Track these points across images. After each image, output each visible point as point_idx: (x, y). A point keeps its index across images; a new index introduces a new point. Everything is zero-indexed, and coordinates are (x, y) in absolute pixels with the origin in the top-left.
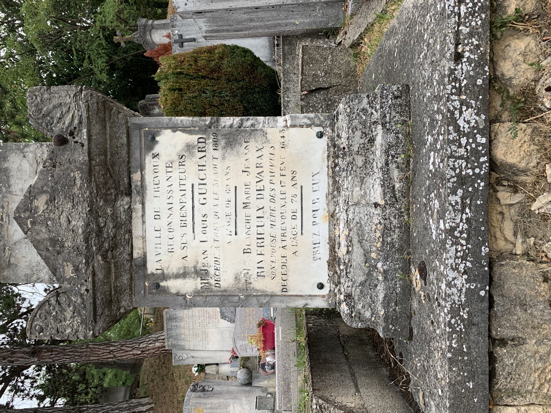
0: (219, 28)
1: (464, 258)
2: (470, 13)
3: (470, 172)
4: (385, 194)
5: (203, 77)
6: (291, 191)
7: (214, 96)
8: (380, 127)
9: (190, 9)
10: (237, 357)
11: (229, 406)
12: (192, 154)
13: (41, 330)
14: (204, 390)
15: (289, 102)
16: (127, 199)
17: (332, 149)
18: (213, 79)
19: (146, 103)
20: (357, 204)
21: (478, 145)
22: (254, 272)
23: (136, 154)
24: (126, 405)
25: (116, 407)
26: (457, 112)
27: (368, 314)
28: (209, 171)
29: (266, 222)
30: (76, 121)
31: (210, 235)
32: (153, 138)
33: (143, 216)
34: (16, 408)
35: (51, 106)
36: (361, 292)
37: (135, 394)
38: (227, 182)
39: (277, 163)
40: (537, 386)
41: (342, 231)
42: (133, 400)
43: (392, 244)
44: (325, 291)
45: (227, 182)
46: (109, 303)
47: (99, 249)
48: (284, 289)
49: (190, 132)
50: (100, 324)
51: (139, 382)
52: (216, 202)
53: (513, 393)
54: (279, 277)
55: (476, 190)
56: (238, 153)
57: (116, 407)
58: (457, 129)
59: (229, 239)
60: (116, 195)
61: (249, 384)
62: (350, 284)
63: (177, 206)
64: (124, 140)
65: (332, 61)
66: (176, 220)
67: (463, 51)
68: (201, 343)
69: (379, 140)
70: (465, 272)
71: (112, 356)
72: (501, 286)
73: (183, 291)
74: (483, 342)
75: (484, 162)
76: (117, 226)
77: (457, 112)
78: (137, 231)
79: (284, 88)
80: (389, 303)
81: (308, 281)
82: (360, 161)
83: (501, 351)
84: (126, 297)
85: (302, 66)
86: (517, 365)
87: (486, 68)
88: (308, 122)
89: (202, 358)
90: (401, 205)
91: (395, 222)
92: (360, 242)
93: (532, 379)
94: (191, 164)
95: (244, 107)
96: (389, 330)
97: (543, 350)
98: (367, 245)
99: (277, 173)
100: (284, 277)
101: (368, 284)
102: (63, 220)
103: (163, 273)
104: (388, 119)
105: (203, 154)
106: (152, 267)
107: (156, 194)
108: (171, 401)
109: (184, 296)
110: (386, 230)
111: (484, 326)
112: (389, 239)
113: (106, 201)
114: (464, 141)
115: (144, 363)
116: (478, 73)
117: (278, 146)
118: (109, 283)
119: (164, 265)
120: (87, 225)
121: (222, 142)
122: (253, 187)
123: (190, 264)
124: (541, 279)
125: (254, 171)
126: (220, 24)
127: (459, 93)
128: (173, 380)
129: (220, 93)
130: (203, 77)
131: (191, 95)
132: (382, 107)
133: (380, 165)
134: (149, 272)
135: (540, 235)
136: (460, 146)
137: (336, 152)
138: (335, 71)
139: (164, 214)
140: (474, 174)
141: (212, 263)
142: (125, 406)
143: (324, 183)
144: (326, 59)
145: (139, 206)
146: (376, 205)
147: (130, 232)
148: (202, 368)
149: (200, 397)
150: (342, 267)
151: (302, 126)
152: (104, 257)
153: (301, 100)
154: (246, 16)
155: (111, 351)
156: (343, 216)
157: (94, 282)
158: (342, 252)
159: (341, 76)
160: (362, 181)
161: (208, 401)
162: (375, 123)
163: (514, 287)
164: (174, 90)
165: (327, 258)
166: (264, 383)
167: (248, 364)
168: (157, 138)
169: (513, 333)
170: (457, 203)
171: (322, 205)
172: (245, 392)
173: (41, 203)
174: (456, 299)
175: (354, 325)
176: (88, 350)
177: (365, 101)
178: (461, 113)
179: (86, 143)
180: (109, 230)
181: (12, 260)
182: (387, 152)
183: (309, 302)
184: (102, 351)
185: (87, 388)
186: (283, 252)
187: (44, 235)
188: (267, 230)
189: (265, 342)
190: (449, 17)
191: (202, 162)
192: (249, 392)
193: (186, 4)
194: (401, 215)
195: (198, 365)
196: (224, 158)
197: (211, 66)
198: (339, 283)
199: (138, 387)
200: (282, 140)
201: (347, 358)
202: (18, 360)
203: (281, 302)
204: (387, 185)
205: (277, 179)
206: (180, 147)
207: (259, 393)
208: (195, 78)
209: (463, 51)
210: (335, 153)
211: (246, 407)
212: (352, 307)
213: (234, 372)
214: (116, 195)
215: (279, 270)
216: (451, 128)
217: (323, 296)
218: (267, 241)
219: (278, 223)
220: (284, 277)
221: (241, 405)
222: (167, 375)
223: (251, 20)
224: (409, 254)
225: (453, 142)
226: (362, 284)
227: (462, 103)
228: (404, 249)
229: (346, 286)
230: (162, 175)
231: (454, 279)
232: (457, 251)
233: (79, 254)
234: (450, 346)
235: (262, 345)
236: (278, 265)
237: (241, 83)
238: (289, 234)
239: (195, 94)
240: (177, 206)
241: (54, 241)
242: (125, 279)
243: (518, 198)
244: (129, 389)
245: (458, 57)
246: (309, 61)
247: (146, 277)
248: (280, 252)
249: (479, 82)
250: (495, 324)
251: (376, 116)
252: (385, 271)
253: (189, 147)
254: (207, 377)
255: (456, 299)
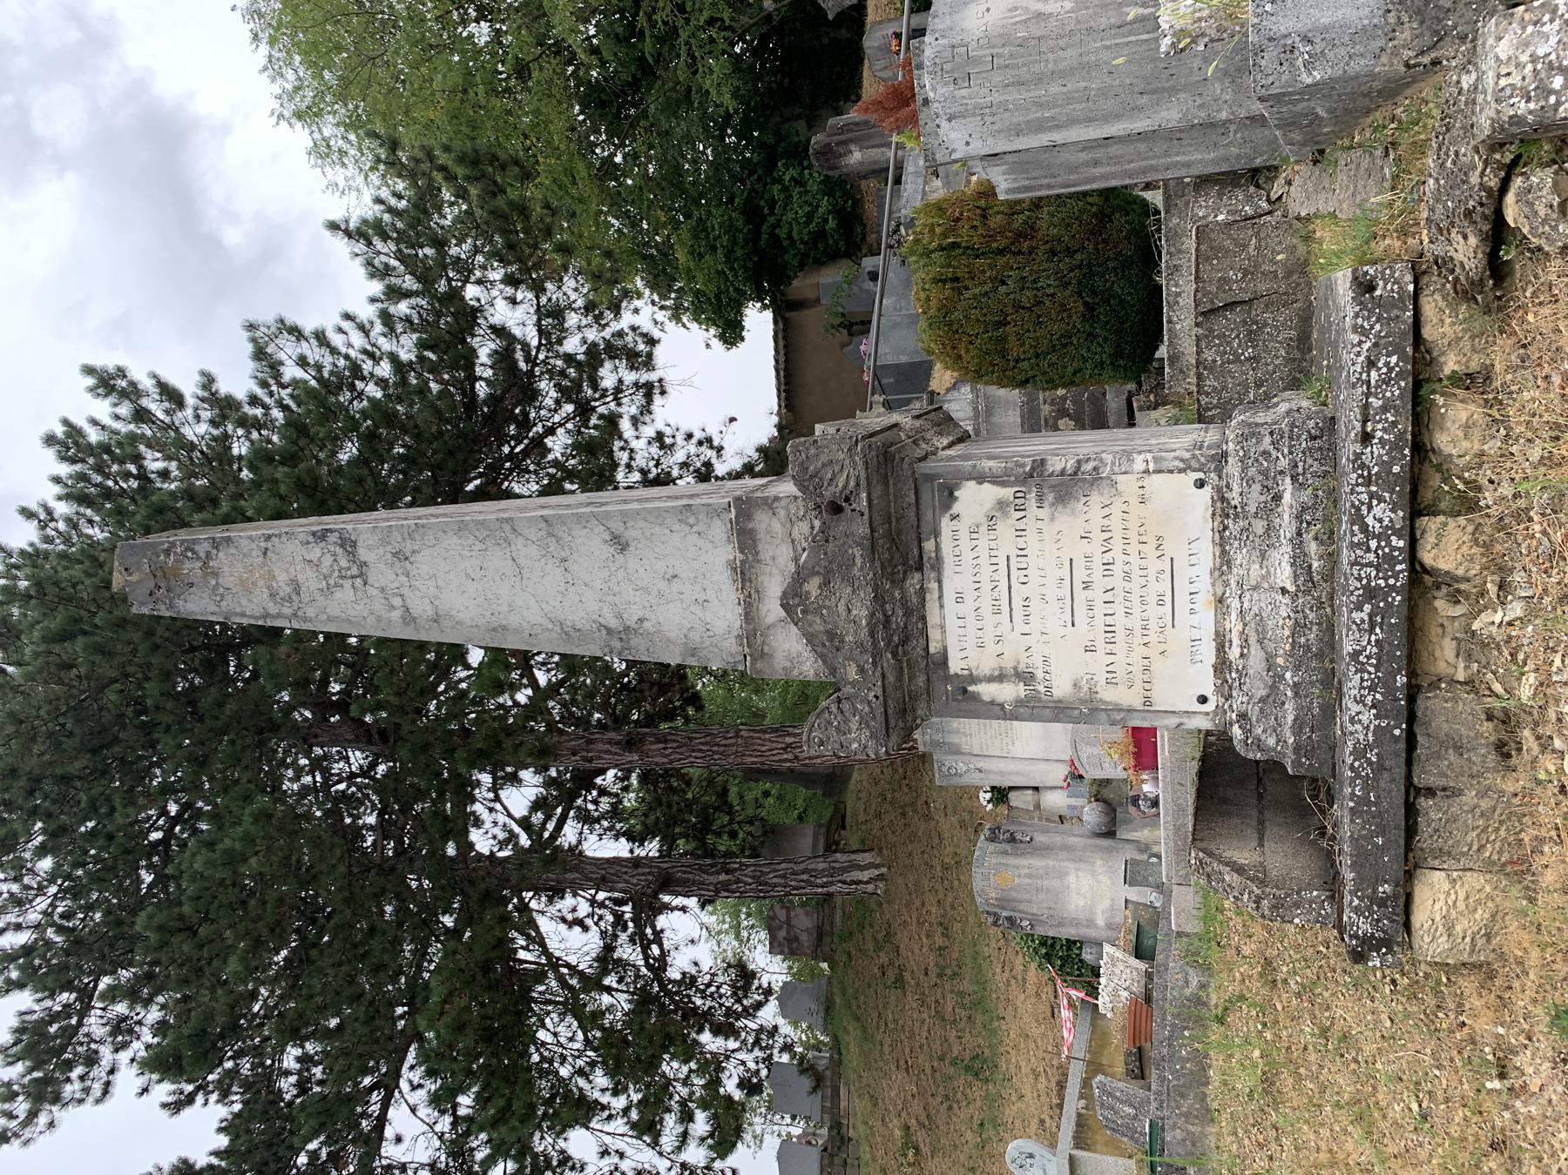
0: (1033, 183)
1: (1372, 689)
2: (1384, 381)
3: (1382, 583)
4: (1296, 577)
5: (1001, 252)
6: (1154, 565)
7: (1022, 289)
8: (1288, 480)
9: (974, 153)
10: (1081, 777)
11: (1067, 874)
12: (1006, 515)
13: (822, 743)
14: (1012, 840)
15: (1178, 294)
16: (917, 576)
17: (1219, 505)
18: (1020, 253)
19: (828, 140)
20: (1255, 588)
21: (1394, 549)
22: (1101, 678)
23: (928, 515)
24: (826, 865)
25: (802, 866)
26: (1364, 508)
27: (1271, 741)
28: (1031, 539)
29: (1119, 609)
30: (852, 483)
31: (1035, 625)
32: (951, 493)
33: (940, 597)
34: (589, 853)
35: (819, 465)
36: (1262, 710)
37: (837, 844)
38: (1059, 553)
39: (1133, 525)
40: (1475, 847)
41: (1233, 624)
42: (838, 855)
43: (1307, 648)
44: (1210, 707)
45: (1059, 553)
46: (903, 712)
47: (888, 645)
48: (1147, 701)
49: (1003, 484)
50: (894, 739)
51: (844, 817)
52: (1042, 581)
53: (1440, 853)
54: (1139, 686)
55: (1390, 605)
56: (1073, 511)
57: (802, 866)
58: (1365, 529)
59: (1063, 631)
60: (905, 572)
61: (1110, 834)
62: (1245, 699)
63: (986, 586)
64: (913, 498)
65: (1258, 248)
66: (986, 605)
67: (1374, 430)
68: (997, 742)
69: (1287, 497)
70: (1374, 706)
71: (790, 756)
72: (1428, 724)
73: (1000, 700)
74: (1398, 791)
75: (1402, 571)
76: (908, 613)
77: (1364, 508)
78: (933, 618)
79: (1168, 267)
80: (1301, 729)
81: (1183, 691)
82: (1259, 526)
83: (1424, 803)
84: (924, 705)
85: (1197, 265)
86: (1447, 821)
87: (1407, 451)
88: (1181, 465)
89: (1001, 773)
90: (1322, 592)
91: (1312, 616)
92: (1260, 642)
93: (1469, 839)
94: (1005, 529)
95: (1086, 304)
96: (1301, 765)
97: (1485, 804)
98: (1271, 646)
99: (1134, 540)
100: (1147, 686)
101: (1271, 699)
102: (842, 608)
103: (971, 674)
104: (1300, 470)
105: (1021, 514)
106: (955, 666)
107: (958, 569)
108: (926, 863)
109: (1002, 706)
110: (1299, 628)
111: (1400, 772)
112: (1303, 640)
113: (893, 582)
114: (1373, 544)
115: (855, 775)
116: (1394, 458)
117: (1134, 501)
118: (902, 687)
119: (972, 664)
120: (872, 615)
121: (1050, 497)
122: (1098, 560)
123: (1008, 663)
124: (1483, 717)
125: (1098, 537)
126: (1035, 174)
127: (1368, 483)
128: (928, 817)
129: (1035, 281)
130: (1001, 252)
131: (977, 291)
132: (1291, 453)
133: (1289, 536)
134: (952, 672)
135: (1484, 661)
136: (1368, 550)
137: (1224, 509)
138: (1265, 267)
139: (970, 596)
140: (1387, 585)
141: (1040, 665)
142: (821, 866)
143: (1206, 553)
144: (1245, 247)
145: (934, 585)
146: (1284, 591)
147: (924, 618)
148: (1001, 794)
149: (1005, 853)
150: (1234, 675)
151: (1171, 472)
152: (895, 655)
153: (1197, 325)
154: (1084, 156)
155: (789, 745)
156: (1235, 604)
157: (884, 686)
158: (1234, 653)
159: (1276, 277)
160: (1263, 556)
161: (1023, 862)
162: (1281, 472)
163: (1445, 725)
164: (944, 281)
165: (1213, 660)
166: (1143, 835)
167: (1106, 793)
168: (957, 494)
169: (1442, 782)
170: (1363, 621)
171: (1205, 585)
172: (1101, 849)
173: (812, 587)
174: (1361, 738)
175: (1250, 756)
176: (740, 741)
177: (1268, 439)
178: (1370, 508)
179: (866, 512)
180: (898, 619)
181: (766, 649)
182: (1299, 518)
183: (1185, 720)
184: (769, 745)
185: (731, 822)
186: (1146, 652)
187: (818, 626)
188: (1120, 621)
189: (1138, 756)
190: (1354, 386)
191: (1021, 525)
192: (1110, 850)
193: (968, 143)
194: (1321, 606)
195: (993, 788)
196: (1052, 519)
197: (1016, 225)
198: (1231, 696)
199: (844, 828)
200: (1141, 492)
201: (1260, 797)
202: (600, 758)
203: (1144, 719)
204: (1300, 562)
205: (1133, 548)
206: (989, 504)
207: (1130, 853)
208: (983, 254)
209: (1374, 430)
210: (1223, 510)
211: (1104, 879)
212: (1247, 732)
213: (1075, 807)
214: (905, 572)
215: (1139, 677)
216: (1356, 528)
217: (1207, 714)
218: (1120, 636)
219: (1136, 611)
220: (1147, 686)
221: (1093, 874)
222: (913, 804)
223: (1096, 163)
224: (1332, 661)
225: (1359, 545)
226: (1263, 700)
227: (1371, 496)
228: (1320, 658)
229: (1239, 701)
230: (965, 544)
231: (1358, 713)
232: (1362, 680)
233: (864, 651)
234: (1353, 793)
235: (1132, 762)
236: (1137, 669)
237: (1078, 256)
238: (1153, 625)
239: (986, 288)
240: (986, 586)
241: (831, 635)
242: (921, 680)
243: (1459, 610)
244: (823, 830)
245: (1366, 438)
246: (1210, 253)
247: (948, 678)
248: (1139, 651)
249: (1396, 469)
250: (1416, 770)
251: (1284, 463)
252: (1295, 684)
253: (1002, 505)
254: (1014, 813)
255: (1361, 738)
